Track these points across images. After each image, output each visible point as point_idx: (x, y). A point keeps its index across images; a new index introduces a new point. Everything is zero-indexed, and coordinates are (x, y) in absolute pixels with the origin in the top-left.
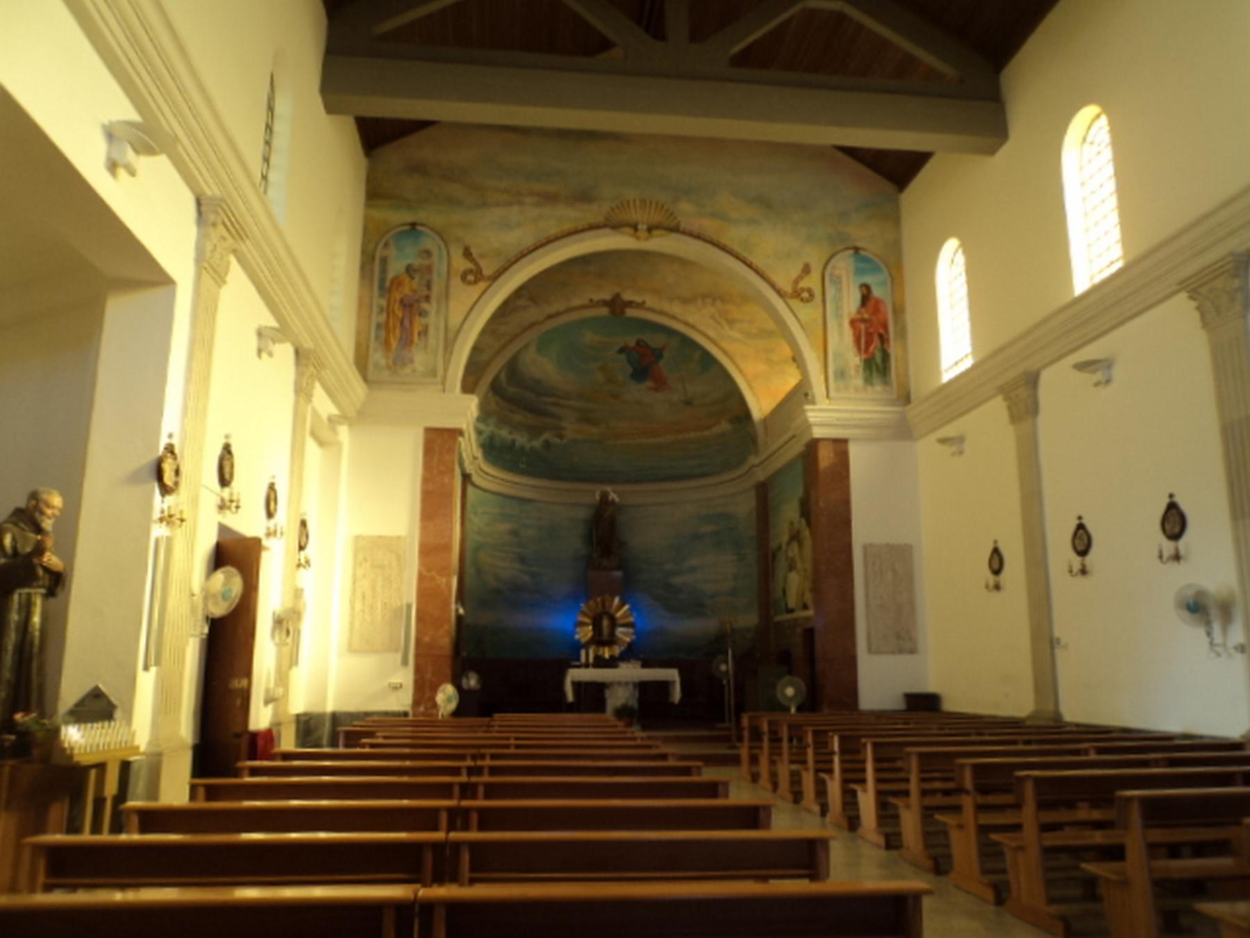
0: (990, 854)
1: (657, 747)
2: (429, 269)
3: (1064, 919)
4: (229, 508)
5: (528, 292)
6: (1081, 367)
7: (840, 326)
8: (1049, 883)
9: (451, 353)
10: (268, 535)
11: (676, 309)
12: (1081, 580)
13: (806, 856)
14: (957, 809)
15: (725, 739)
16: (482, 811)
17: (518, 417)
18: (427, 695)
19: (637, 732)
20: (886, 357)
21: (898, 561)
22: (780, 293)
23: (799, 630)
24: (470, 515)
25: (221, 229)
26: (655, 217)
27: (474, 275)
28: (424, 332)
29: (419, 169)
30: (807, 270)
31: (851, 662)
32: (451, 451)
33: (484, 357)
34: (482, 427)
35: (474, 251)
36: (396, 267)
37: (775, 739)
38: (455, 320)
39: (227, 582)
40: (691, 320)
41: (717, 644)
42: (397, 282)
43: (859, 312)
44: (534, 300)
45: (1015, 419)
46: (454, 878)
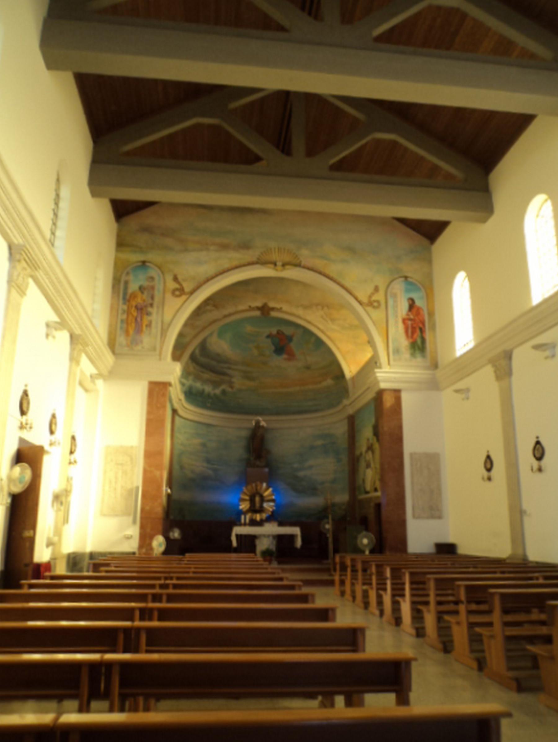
0: (475, 640)
1: (278, 573)
2: (153, 288)
3: (517, 680)
4: (26, 428)
5: (211, 302)
6: (537, 347)
7: (396, 322)
8: (509, 659)
9: (165, 336)
10: (51, 444)
11: (300, 312)
12: (538, 475)
13: (352, 638)
14: (456, 612)
15: (327, 571)
16: (160, 610)
17: (207, 375)
18: (148, 541)
19: (275, 565)
20: (423, 340)
21: (431, 463)
22: (360, 303)
23: (372, 504)
24: (177, 434)
25: (24, 264)
26: (287, 258)
27: (179, 292)
28: (149, 325)
29: (147, 230)
30: (376, 289)
31: (403, 523)
32: (164, 395)
33: (187, 339)
34: (184, 381)
35: (180, 278)
36: (133, 287)
37: (354, 571)
38: (168, 317)
39: (22, 472)
40: (309, 318)
41: (323, 513)
42: (134, 296)
43: (408, 315)
44: (216, 306)
45: (498, 378)
46: (136, 650)
